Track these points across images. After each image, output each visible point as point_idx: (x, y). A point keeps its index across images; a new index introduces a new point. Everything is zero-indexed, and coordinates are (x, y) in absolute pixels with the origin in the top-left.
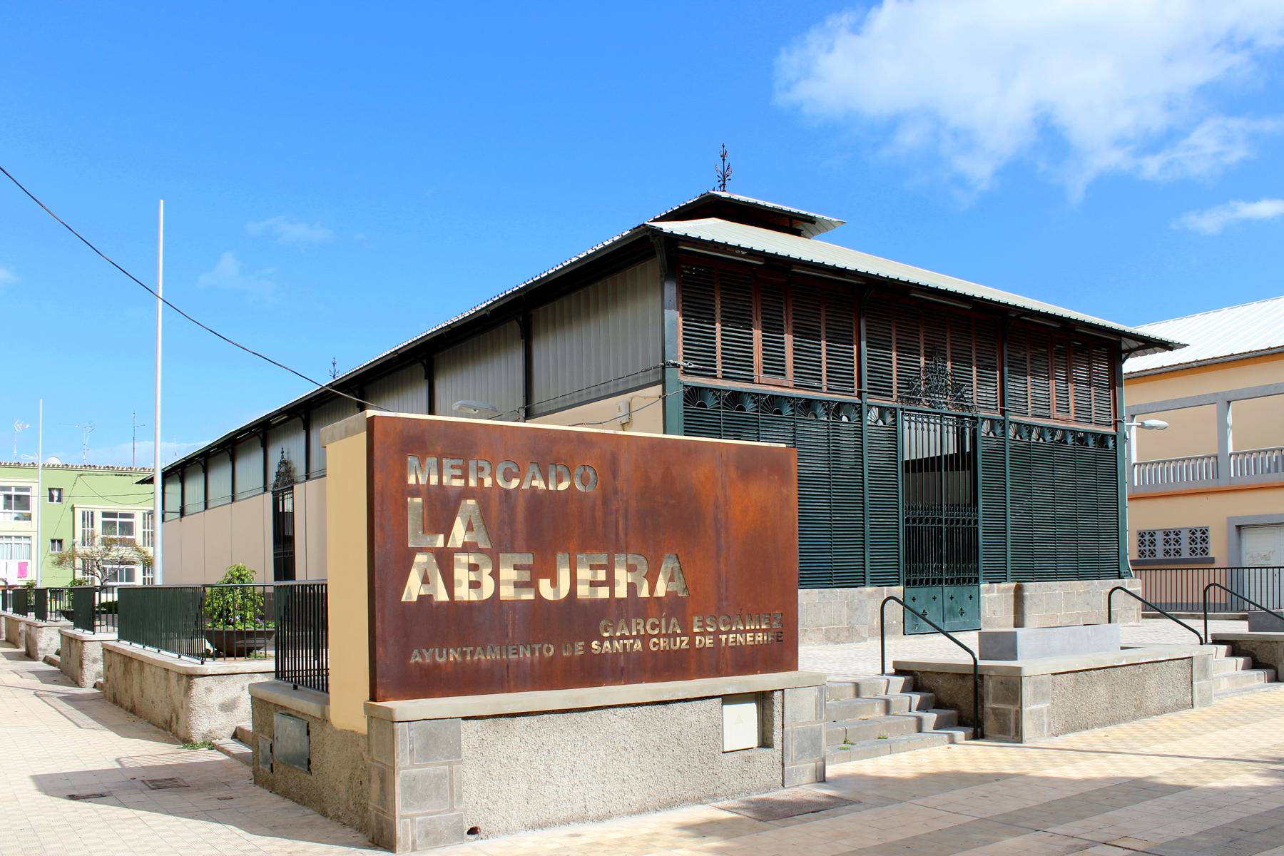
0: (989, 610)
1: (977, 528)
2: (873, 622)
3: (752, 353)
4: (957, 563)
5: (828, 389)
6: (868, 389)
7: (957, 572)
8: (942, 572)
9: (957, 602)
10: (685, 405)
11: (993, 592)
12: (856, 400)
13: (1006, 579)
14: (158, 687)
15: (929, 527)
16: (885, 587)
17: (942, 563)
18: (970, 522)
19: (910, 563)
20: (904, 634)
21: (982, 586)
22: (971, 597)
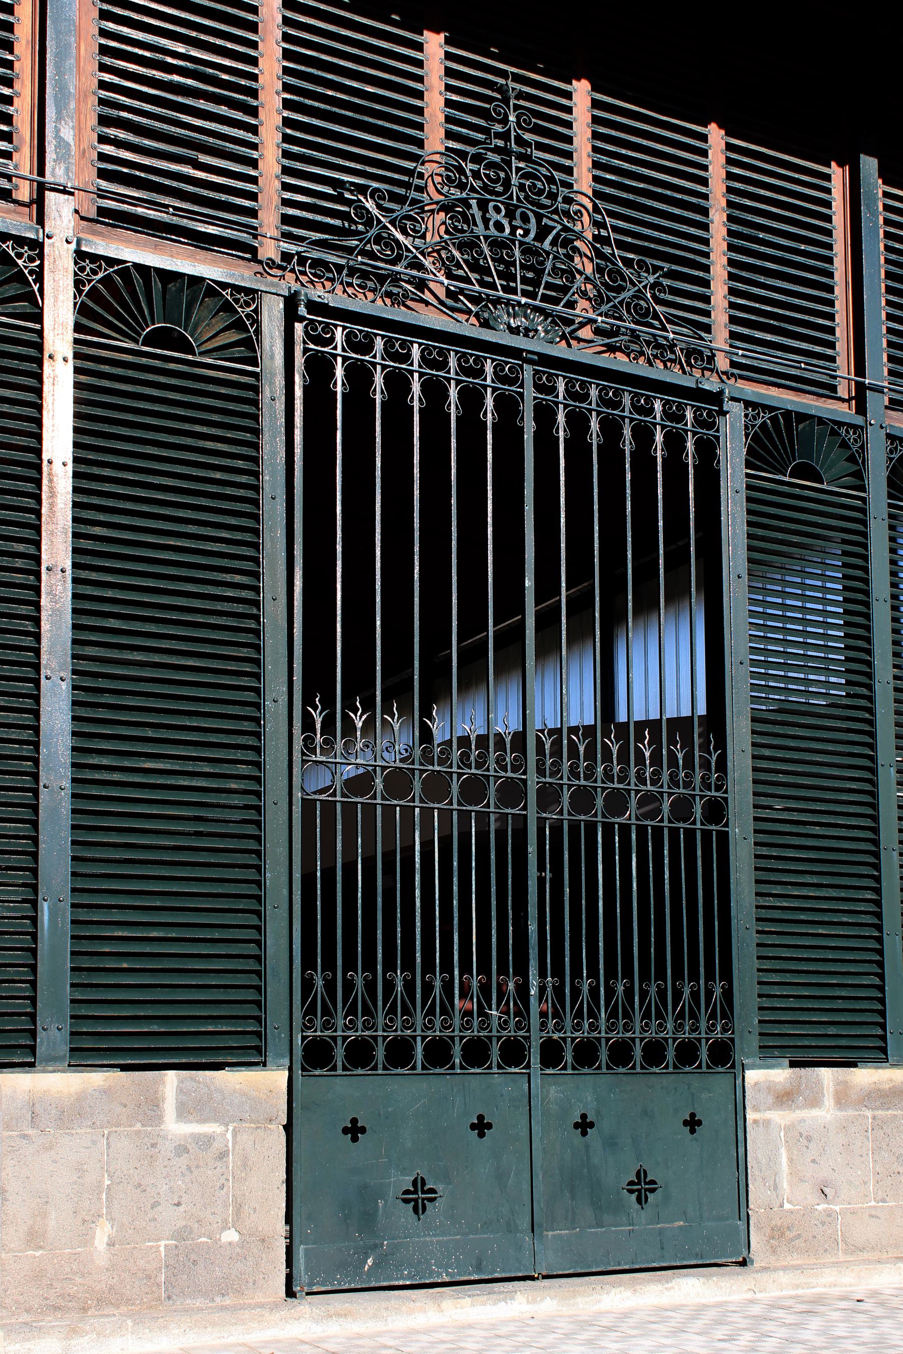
0: (797, 1177)
1: (724, 838)
2: (87, 1238)
3: (286, 203)
4: (611, 974)
5: (733, 364)
6: (731, 346)
7: (613, 1015)
8: (523, 1012)
9: (611, 1143)
10: (890, 496)
11: (815, 1102)
12: (844, 411)
13: (884, 1050)
14: (28, 1166)
15: (446, 815)
16: (171, 1075)
17: (522, 970)
18: (682, 809)
19: (329, 964)
20: (290, 1293)
21: (752, 1076)
22: (693, 1123)
